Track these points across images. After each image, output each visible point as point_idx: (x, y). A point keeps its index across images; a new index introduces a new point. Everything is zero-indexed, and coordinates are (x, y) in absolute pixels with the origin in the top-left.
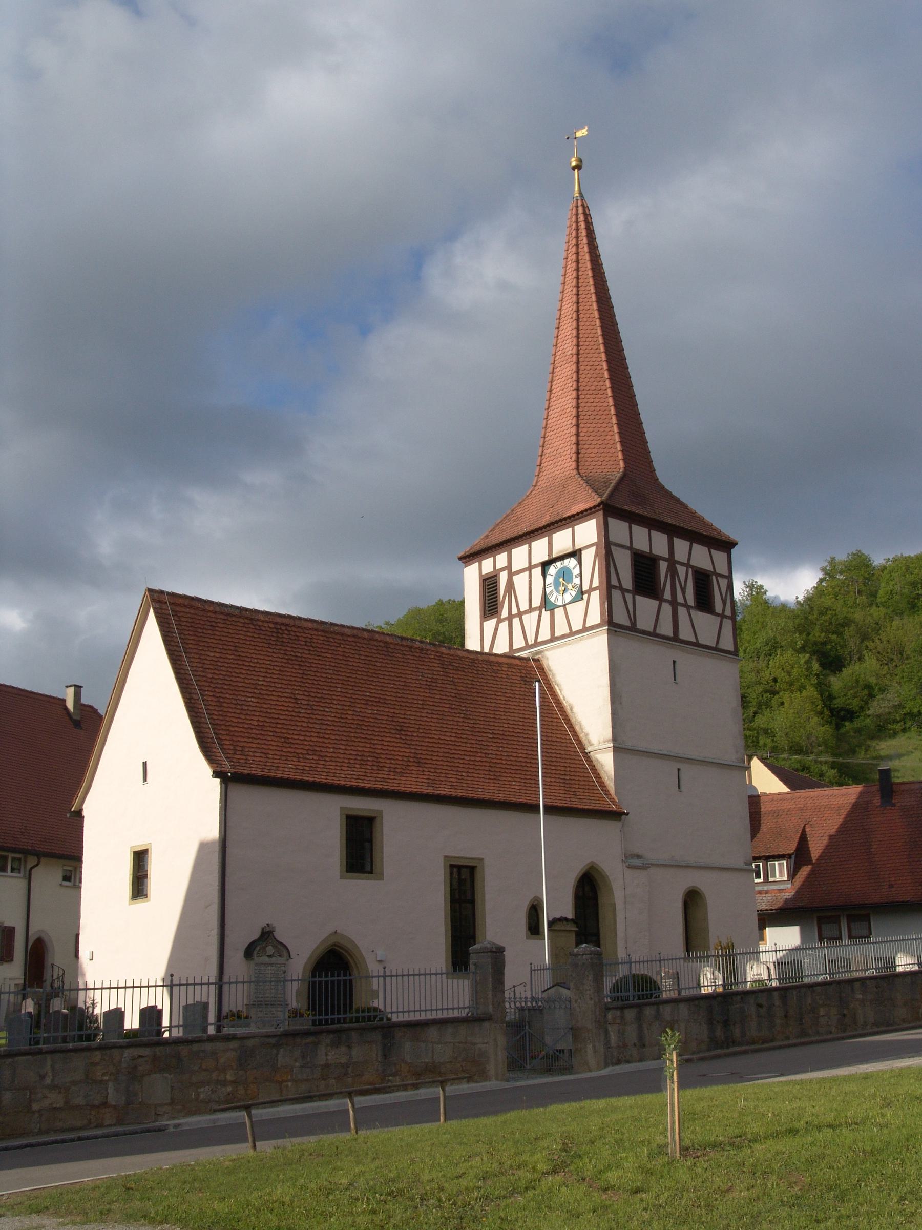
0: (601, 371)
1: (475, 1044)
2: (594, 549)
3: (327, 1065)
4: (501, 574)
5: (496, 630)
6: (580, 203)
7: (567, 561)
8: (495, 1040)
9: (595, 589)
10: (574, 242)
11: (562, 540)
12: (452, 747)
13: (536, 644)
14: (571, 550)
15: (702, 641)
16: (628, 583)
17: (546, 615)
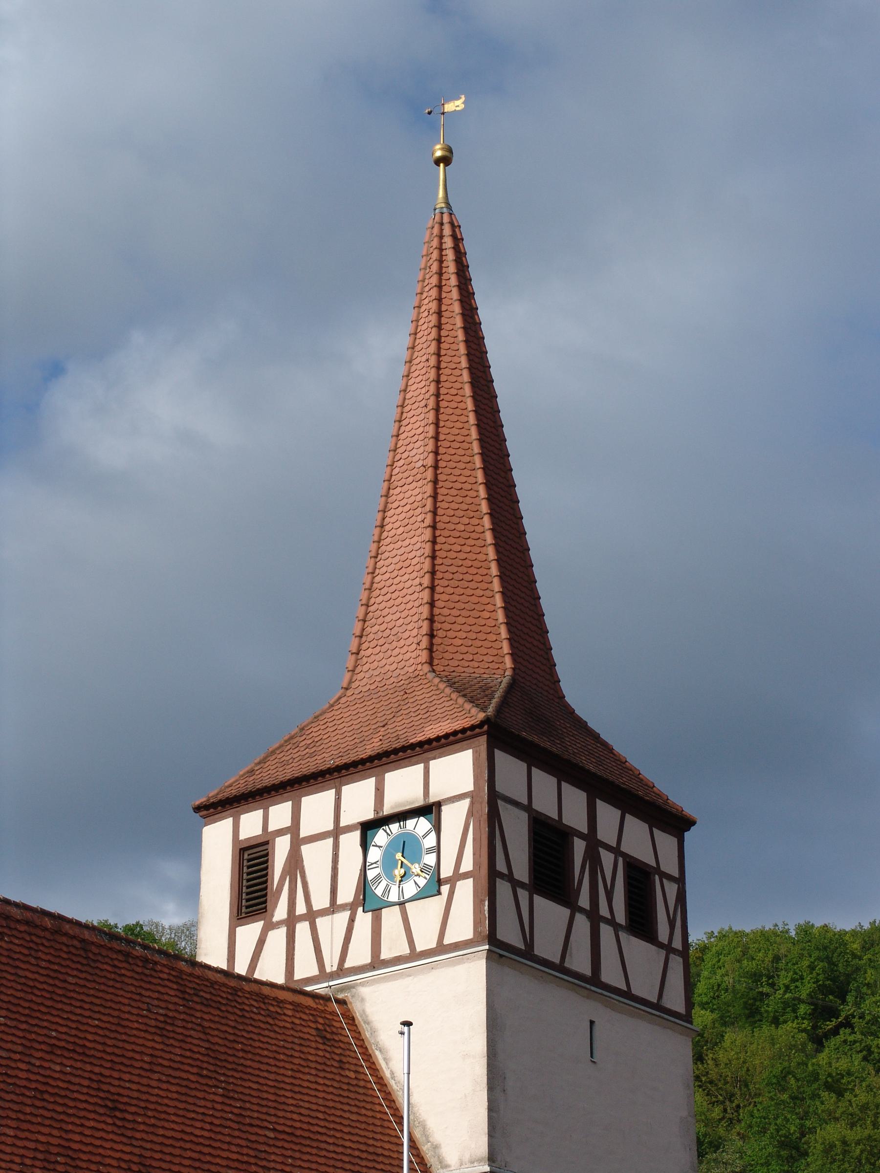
0: (475, 501)
2: (466, 803)
4: (278, 840)
5: (261, 942)
6: (446, 219)
7: (410, 823)
9: (466, 876)
10: (434, 280)
11: (403, 785)
12: (206, 1150)
13: (342, 971)
14: (420, 802)
15: (636, 991)
16: (522, 873)
17: (364, 920)
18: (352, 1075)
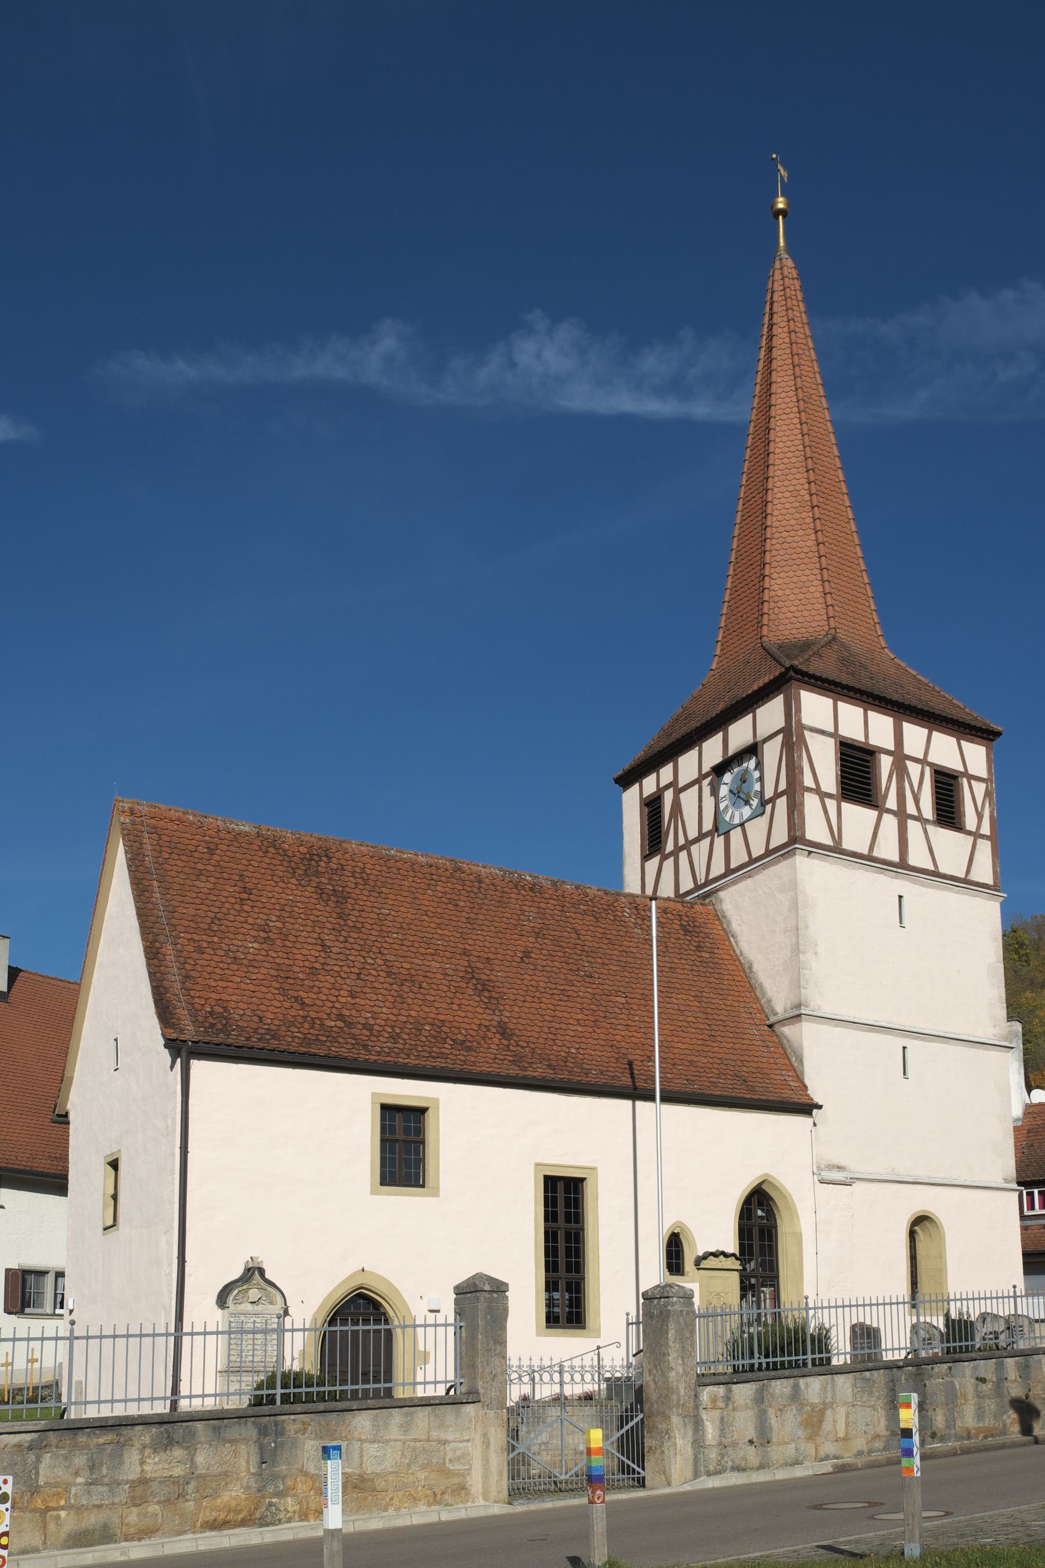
1: (445, 1442)
3: (144, 1481)
8: (485, 1435)
11: (740, 733)
15: (943, 869)
17: (720, 841)
18: (708, 955)
